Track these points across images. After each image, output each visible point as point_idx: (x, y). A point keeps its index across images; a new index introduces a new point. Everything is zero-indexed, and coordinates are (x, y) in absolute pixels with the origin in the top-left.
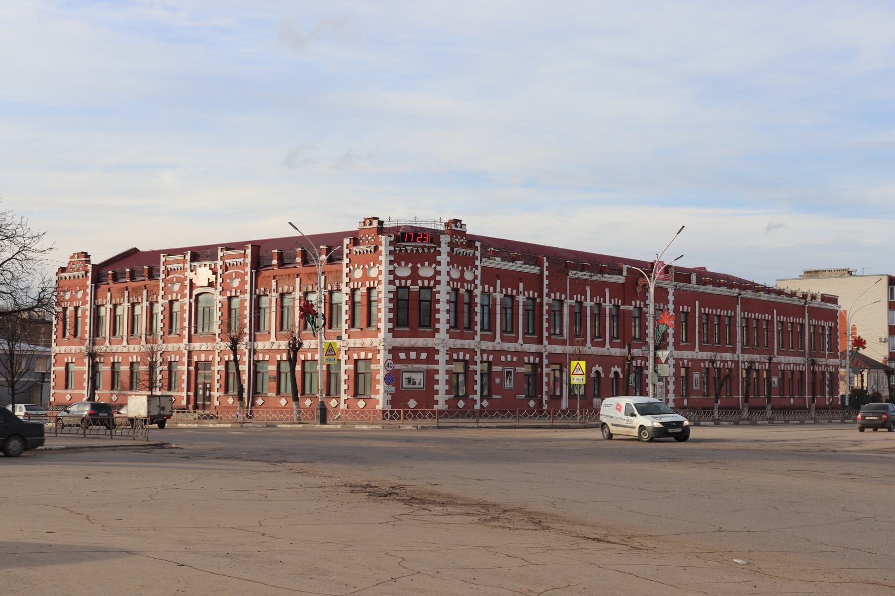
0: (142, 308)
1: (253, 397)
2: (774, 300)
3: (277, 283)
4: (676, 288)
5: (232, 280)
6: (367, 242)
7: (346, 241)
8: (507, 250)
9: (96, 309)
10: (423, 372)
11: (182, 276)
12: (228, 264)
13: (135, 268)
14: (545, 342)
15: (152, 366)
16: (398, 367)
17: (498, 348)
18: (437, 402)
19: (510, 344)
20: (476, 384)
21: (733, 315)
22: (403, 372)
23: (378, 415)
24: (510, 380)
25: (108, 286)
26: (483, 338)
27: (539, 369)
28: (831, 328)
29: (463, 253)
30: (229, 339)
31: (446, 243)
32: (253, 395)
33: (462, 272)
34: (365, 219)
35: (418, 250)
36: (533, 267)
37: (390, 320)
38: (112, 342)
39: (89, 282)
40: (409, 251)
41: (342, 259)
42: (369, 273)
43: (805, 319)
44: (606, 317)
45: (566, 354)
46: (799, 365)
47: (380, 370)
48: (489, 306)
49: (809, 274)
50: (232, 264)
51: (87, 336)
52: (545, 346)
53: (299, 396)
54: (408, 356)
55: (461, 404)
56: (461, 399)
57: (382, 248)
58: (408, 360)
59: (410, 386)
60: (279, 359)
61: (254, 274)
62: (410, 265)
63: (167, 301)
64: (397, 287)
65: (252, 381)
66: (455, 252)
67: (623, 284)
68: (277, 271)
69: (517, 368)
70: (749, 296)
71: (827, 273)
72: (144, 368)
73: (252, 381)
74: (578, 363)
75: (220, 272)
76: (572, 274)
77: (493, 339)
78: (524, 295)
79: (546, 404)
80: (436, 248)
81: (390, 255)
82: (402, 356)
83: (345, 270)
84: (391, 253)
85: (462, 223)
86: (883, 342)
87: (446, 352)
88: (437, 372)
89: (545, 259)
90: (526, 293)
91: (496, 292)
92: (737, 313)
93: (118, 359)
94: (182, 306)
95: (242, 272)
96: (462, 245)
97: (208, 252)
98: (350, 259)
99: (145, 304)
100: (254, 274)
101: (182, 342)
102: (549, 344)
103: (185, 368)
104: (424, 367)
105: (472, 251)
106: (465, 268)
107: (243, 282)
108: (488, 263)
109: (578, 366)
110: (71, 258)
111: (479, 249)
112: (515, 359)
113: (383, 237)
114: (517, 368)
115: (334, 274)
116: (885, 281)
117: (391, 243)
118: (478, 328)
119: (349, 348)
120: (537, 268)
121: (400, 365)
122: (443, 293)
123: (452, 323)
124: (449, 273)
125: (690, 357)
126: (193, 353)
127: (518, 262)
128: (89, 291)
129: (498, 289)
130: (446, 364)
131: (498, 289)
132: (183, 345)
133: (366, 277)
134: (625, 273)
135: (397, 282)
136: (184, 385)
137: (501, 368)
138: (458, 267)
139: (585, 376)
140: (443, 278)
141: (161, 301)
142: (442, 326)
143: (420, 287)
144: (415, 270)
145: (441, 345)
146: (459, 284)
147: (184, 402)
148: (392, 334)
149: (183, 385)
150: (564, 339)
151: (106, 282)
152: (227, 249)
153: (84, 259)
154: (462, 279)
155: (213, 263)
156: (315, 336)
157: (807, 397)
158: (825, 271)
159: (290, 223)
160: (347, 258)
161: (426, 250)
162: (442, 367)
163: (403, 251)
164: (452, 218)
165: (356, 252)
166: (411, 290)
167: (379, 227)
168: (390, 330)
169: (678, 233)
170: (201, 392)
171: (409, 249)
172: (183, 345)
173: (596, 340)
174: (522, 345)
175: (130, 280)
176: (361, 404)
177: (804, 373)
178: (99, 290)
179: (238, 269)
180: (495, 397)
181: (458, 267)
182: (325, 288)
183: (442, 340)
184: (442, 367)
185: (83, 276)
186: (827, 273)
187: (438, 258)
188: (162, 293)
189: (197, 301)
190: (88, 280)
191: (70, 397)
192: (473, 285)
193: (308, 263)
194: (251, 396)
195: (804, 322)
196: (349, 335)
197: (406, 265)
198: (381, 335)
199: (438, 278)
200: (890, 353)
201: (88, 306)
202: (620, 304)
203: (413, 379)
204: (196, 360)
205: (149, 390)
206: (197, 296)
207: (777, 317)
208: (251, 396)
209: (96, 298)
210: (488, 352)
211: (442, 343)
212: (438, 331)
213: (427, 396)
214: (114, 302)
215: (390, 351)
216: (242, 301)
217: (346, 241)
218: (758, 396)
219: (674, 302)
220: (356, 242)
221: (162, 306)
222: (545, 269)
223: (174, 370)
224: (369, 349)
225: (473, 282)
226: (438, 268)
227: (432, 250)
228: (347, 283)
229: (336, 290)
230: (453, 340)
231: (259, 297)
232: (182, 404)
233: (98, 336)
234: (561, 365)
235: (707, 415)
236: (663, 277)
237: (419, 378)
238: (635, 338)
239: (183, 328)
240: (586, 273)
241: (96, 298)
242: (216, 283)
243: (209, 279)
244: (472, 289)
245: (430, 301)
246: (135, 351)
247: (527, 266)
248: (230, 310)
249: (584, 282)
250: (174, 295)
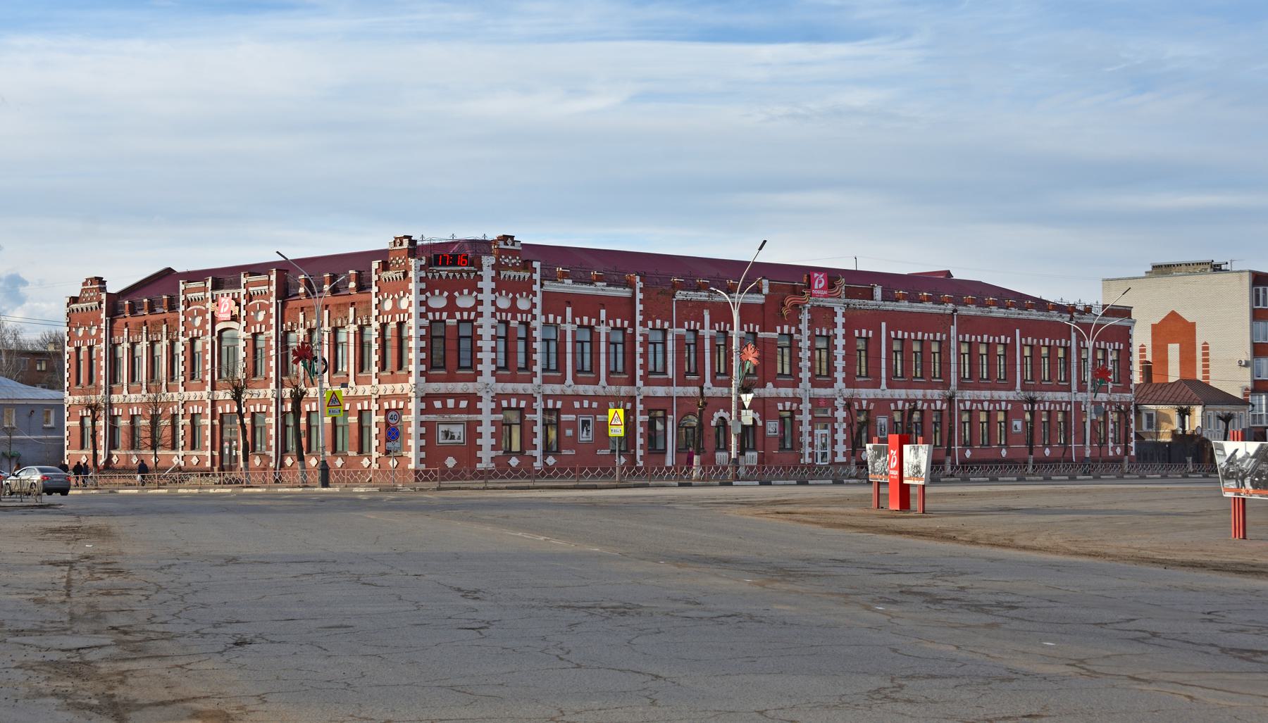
0: (162, 347)
1: (282, 456)
2: (1016, 316)
3: (304, 317)
4: (848, 306)
5: (257, 313)
6: (397, 266)
7: (375, 265)
8: (582, 270)
9: (113, 349)
10: (464, 424)
11: (204, 308)
12: (252, 294)
13: (155, 297)
14: (639, 383)
15: (154, 419)
16: (432, 417)
17: (569, 391)
18: (480, 460)
19: (587, 387)
20: (536, 437)
21: (944, 339)
22: (438, 424)
23: (410, 476)
24: (588, 431)
25: (125, 320)
26: (546, 380)
29: (515, 276)
30: (231, 388)
31: (489, 266)
32: (282, 453)
33: (514, 300)
34: (396, 238)
35: (454, 275)
36: (622, 289)
37: (422, 362)
38: (169, 390)
39: (103, 316)
40: (444, 277)
41: (371, 287)
42: (399, 304)
43: (1070, 339)
44: (710, 349)
45: (673, 397)
46: (1060, 403)
47: (412, 420)
48: (556, 340)
49: (1159, 270)
50: (256, 293)
51: (103, 383)
52: (639, 388)
53: (304, 454)
54: (444, 404)
55: (514, 462)
56: (514, 456)
57: (412, 274)
58: (445, 410)
59: (448, 441)
60: (359, 408)
61: (280, 305)
62: (446, 294)
63: (187, 339)
64: (430, 321)
65: (280, 436)
66: (502, 277)
67: (763, 305)
68: (304, 301)
69: (597, 416)
70: (973, 313)
71: (1184, 267)
72: (144, 422)
73: (280, 436)
74: (616, 411)
75: (243, 302)
76: (680, 295)
77: (562, 380)
78: (608, 324)
79: (641, 460)
80: (476, 273)
81: (420, 282)
82: (438, 404)
83: (375, 301)
84: (422, 279)
85: (515, 239)
86: (1244, 366)
87: (490, 399)
88: (480, 423)
89: (638, 278)
90: (611, 322)
91: (565, 323)
92: (952, 335)
93: (118, 412)
94: (204, 345)
95: (267, 303)
96: (514, 268)
97: (229, 278)
98: (379, 287)
99: (165, 342)
100: (280, 305)
101: (268, 387)
102: (645, 385)
103: (208, 422)
104: (465, 417)
105: (527, 275)
106: (518, 295)
107: (268, 316)
108: (551, 287)
109: (616, 415)
110: (85, 284)
111: (538, 270)
112: (595, 405)
113: (413, 260)
114: (597, 416)
115: (364, 306)
116: (1247, 280)
117: (422, 267)
118: (537, 369)
119: (380, 396)
120: (627, 289)
121: (434, 416)
122: (487, 327)
123: (502, 363)
124: (494, 303)
125: (872, 397)
126: (217, 403)
127: (598, 284)
128: (103, 326)
129: (569, 318)
130: (492, 414)
131: (569, 318)
132: (205, 394)
133: (396, 309)
134: (766, 290)
135: (430, 315)
136: (208, 443)
137: (574, 416)
138: (507, 294)
139: (623, 427)
140: (487, 309)
141: (182, 339)
142: (486, 367)
143: (458, 320)
144: (451, 299)
146: (510, 315)
147: (208, 464)
148: (424, 378)
149: (206, 442)
150: (668, 379)
151: (122, 316)
152: (252, 274)
153: (97, 286)
154: (514, 309)
155: (236, 291)
156: (313, 384)
157: (1073, 445)
158: (1181, 265)
159: (278, 252)
160: (376, 285)
161: (465, 275)
162: (486, 417)
163: (437, 277)
164: (501, 234)
165: (385, 279)
166: (447, 324)
167: (410, 247)
168: (422, 374)
169: (760, 249)
170: (227, 452)
171: (444, 274)
172: (205, 394)
173: (719, 378)
174: (604, 387)
175: (149, 313)
176: (392, 463)
177: (1069, 413)
178: (115, 325)
179: (263, 299)
180: (565, 452)
181: (507, 294)
182: (355, 322)
183: (486, 383)
184: (486, 417)
185: (96, 308)
186: (1184, 267)
187: (480, 285)
188: (182, 329)
189: (220, 338)
190: (102, 313)
191: (86, 459)
192: (529, 316)
193: (339, 291)
194: (279, 456)
195: (1069, 345)
196: (379, 380)
197: (441, 293)
198: (412, 380)
199: (480, 309)
200: (1255, 382)
201: (103, 345)
202: (757, 330)
203: (452, 433)
204: (220, 411)
205: (152, 449)
206: (221, 332)
207: (1021, 340)
208: (279, 456)
209: (111, 335)
210: (555, 397)
211: (486, 388)
212: (480, 373)
213: (469, 451)
214: (131, 340)
215: (423, 399)
216: (268, 340)
217: (375, 265)
218: (988, 445)
219: (844, 326)
220: (385, 266)
221: (183, 345)
222: (638, 291)
223: (197, 425)
224: (400, 396)
225: (530, 311)
226: (480, 297)
227: (472, 275)
228: (376, 316)
229: (366, 325)
230: (500, 385)
231: (286, 333)
232: (207, 466)
233: (115, 382)
234: (665, 411)
235: (1066, 469)
236: (825, 292)
237: (458, 430)
238: (782, 374)
239: (205, 372)
240: (703, 294)
241: (111, 335)
242: (240, 316)
243: (232, 312)
244: (529, 320)
246: (197, 399)
247: (612, 288)
248: (255, 350)
249: (701, 305)
250: (195, 331)
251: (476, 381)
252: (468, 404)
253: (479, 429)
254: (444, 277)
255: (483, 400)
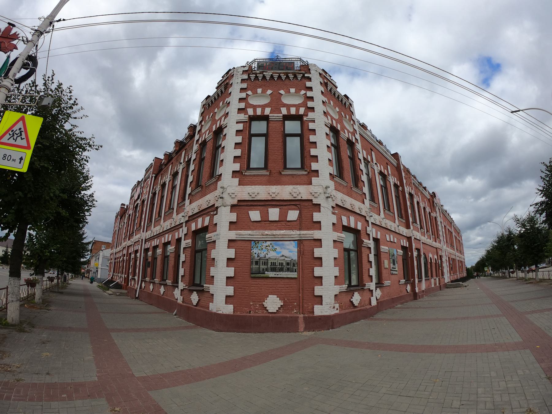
16: (246, 234)
18: (319, 299)
27: (410, 254)
28: (360, 286)
54: (264, 215)
56: (356, 291)
58: (265, 223)
64: (249, 116)
88: (318, 242)
104: (295, 234)
145: (323, 196)
194: (140, 280)
197: (264, 92)
208: (140, 280)
245: (301, 136)
251: (310, 183)
252: (300, 214)
253: (317, 252)
254: (268, 78)
255: (322, 209)
